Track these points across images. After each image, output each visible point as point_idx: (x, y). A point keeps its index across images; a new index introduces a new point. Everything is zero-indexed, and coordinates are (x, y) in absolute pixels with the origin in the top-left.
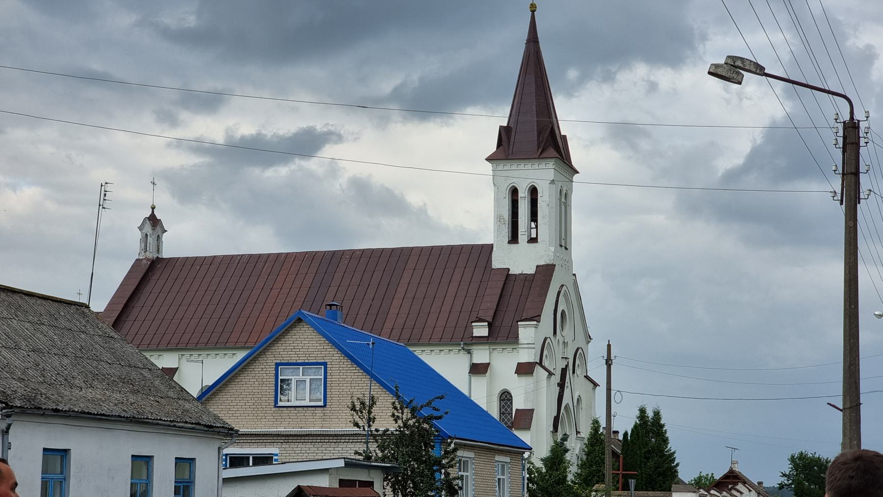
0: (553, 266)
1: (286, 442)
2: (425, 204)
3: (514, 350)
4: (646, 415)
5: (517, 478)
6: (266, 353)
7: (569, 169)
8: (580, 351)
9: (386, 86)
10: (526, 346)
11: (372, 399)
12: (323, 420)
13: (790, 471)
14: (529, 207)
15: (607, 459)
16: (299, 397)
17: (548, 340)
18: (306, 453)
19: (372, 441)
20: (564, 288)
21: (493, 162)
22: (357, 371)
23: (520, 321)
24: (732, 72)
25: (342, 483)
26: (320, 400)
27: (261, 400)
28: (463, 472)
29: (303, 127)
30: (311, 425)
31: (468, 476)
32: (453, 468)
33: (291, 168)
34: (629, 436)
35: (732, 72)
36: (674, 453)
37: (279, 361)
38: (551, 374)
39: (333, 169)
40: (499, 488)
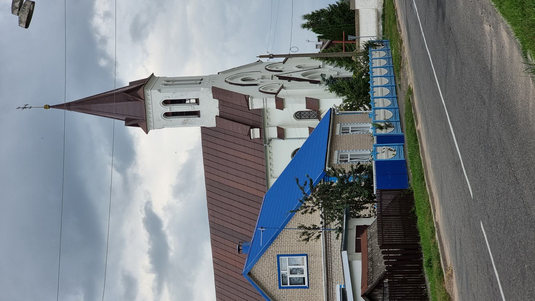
0: (213, 88)
1: (332, 280)
2: (187, 151)
3: (268, 111)
4: (306, 24)
5: (351, 118)
6: (273, 295)
7: (151, 79)
8: (267, 67)
9: (117, 177)
10: (265, 103)
11: (300, 227)
12: (316, 256)
14: (176, 105)
15: (335, 55)
16: (301, 281)
17: (261, 89)
18: (339, 267)
19: (329, 226)
20: (227, 80)
21: (148, 129)
22: (282, 234)
23: (249, 108)
24: (24, 10)
25: (358, 250)
26: (303, 259)
27: (304, 298)
28: (349, 130)
29: (143, 226)
30: (320, 264)
31: (350, 155)
32: (345, 170)
33: (169, 234)
34: (320, 35)
35: (24, 10)
36: (330, 5)
37: (278, 287)
38: (282, 87)
39: (168, 208)
40: (357, 131)
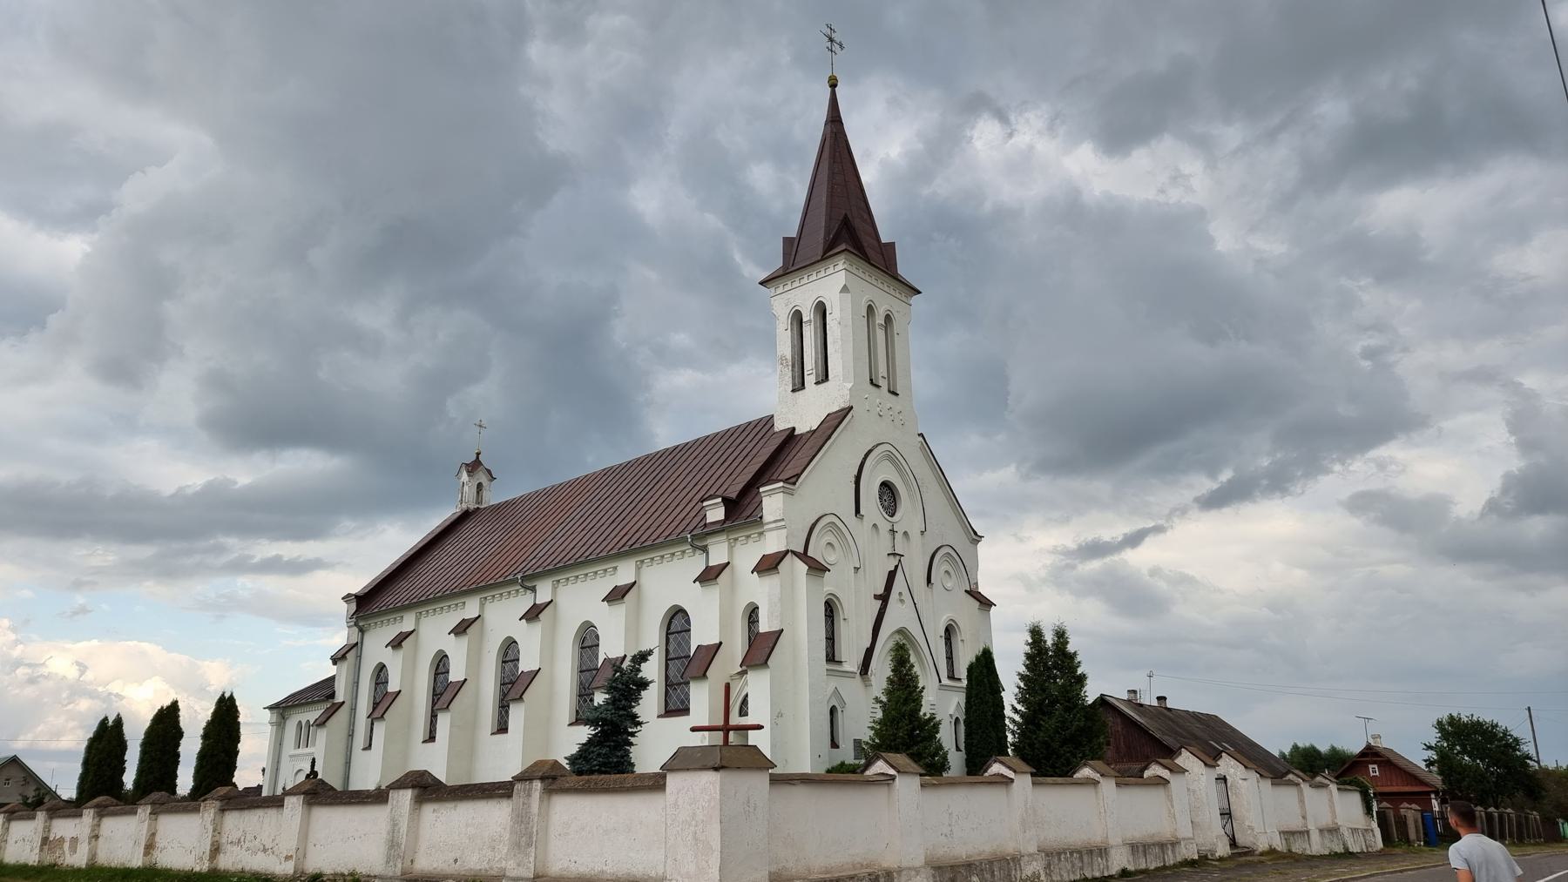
10: (774, 525)
13: (1438, 742)
